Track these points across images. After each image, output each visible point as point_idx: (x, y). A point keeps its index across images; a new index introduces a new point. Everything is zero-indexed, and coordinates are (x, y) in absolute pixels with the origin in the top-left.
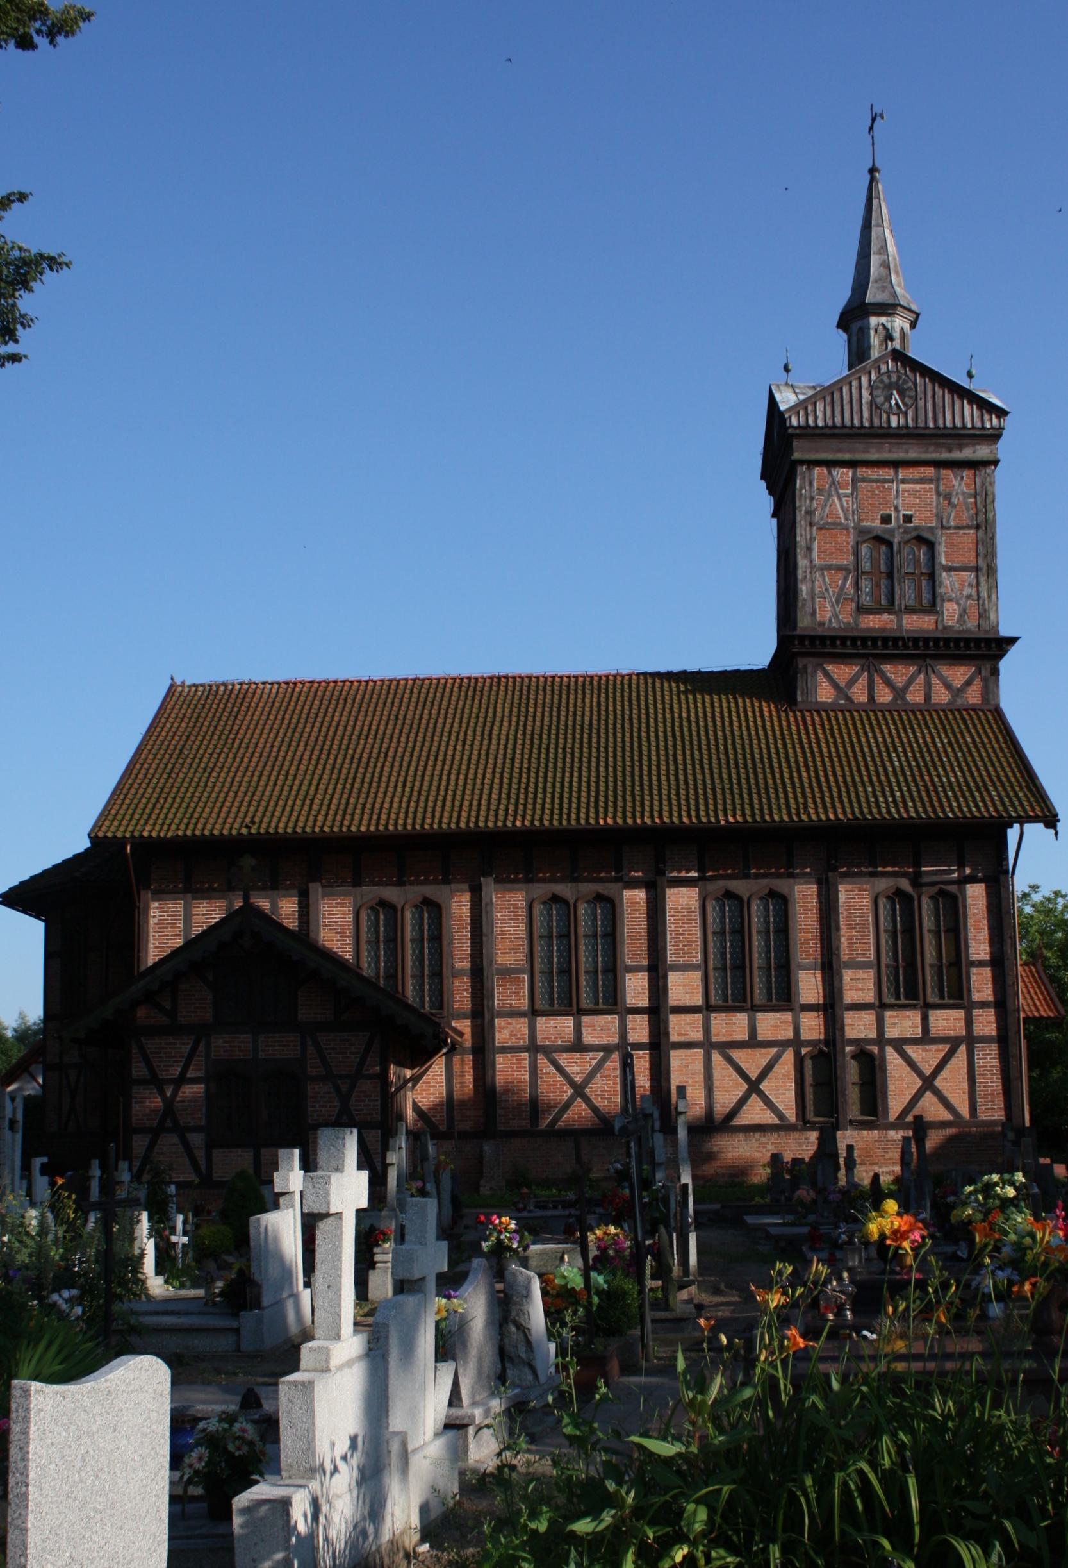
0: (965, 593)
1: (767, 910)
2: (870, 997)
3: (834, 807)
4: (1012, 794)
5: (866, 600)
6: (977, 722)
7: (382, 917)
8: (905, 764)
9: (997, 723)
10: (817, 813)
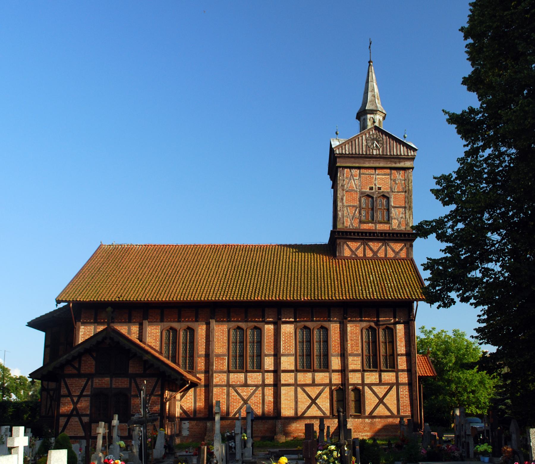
0: (400, 216)
1: (320, 333)
2: (359, 367)
3: (346, 294)
4: (414, 290)
5: (363, 218)
6: (404, 264)
7: (171, 334)
8: (375, 279)
9: (411, 265)
10: (339, 297)
